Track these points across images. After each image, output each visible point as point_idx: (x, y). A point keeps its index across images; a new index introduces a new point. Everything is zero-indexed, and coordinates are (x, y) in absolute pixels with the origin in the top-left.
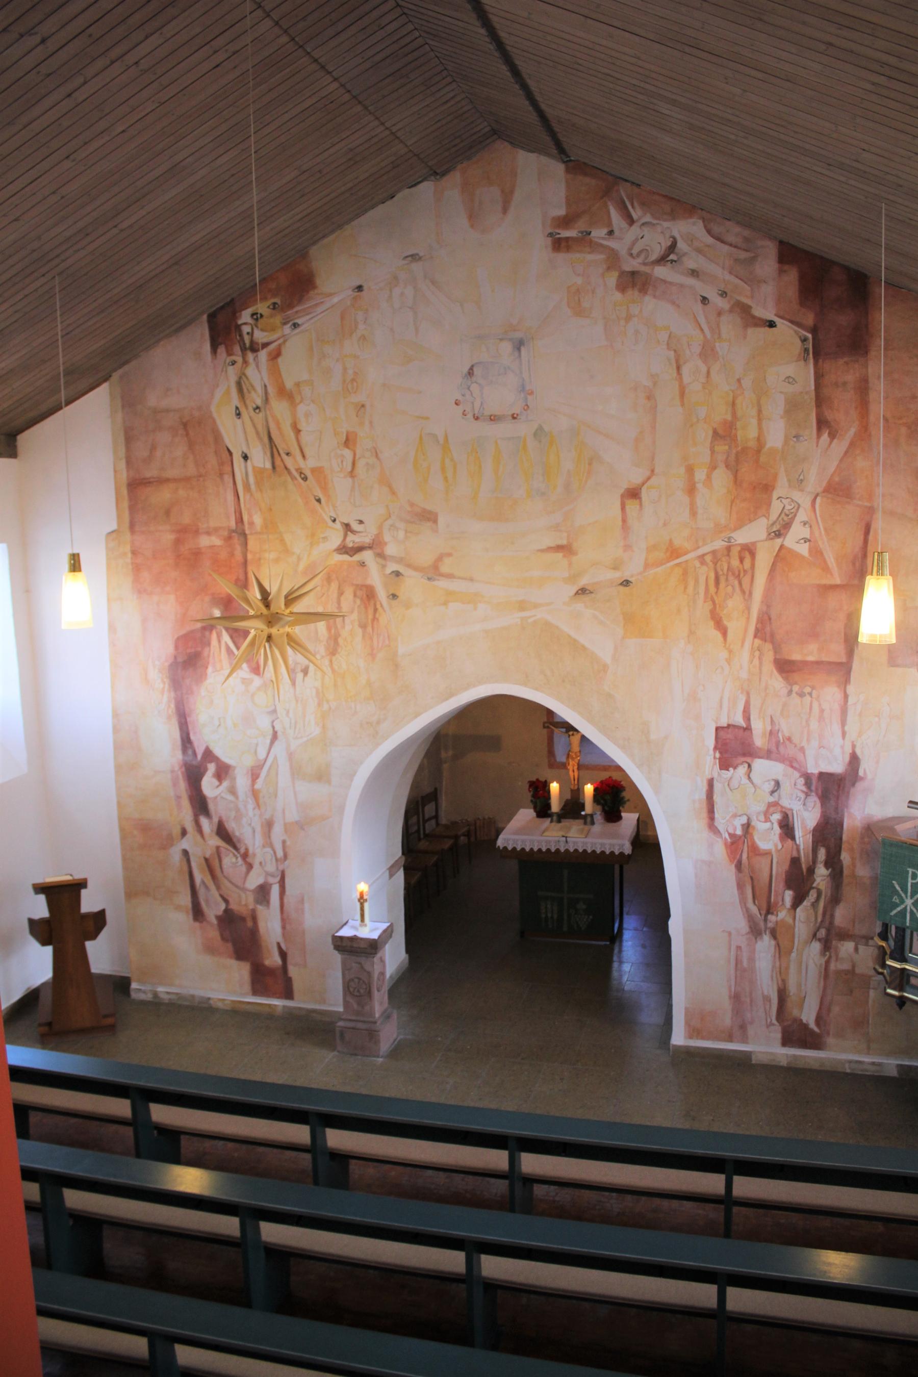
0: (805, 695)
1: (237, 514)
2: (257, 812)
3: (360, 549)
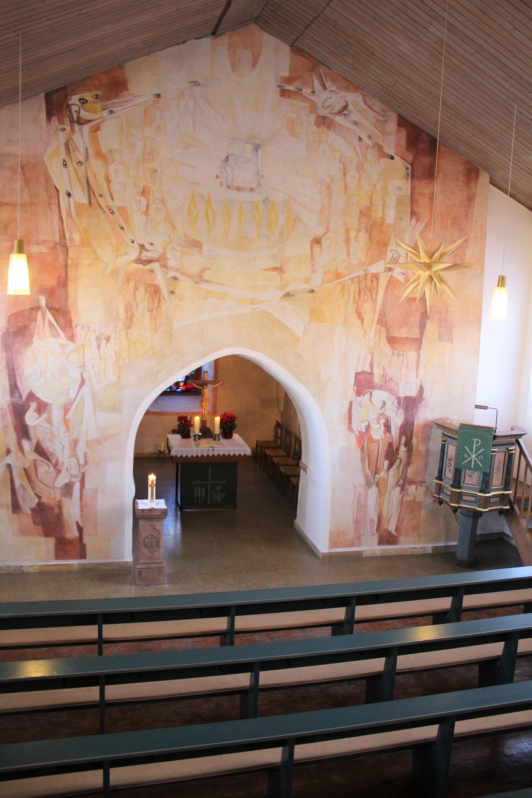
0: (400, 356)
1: (61, 233)
3: (150, 261)
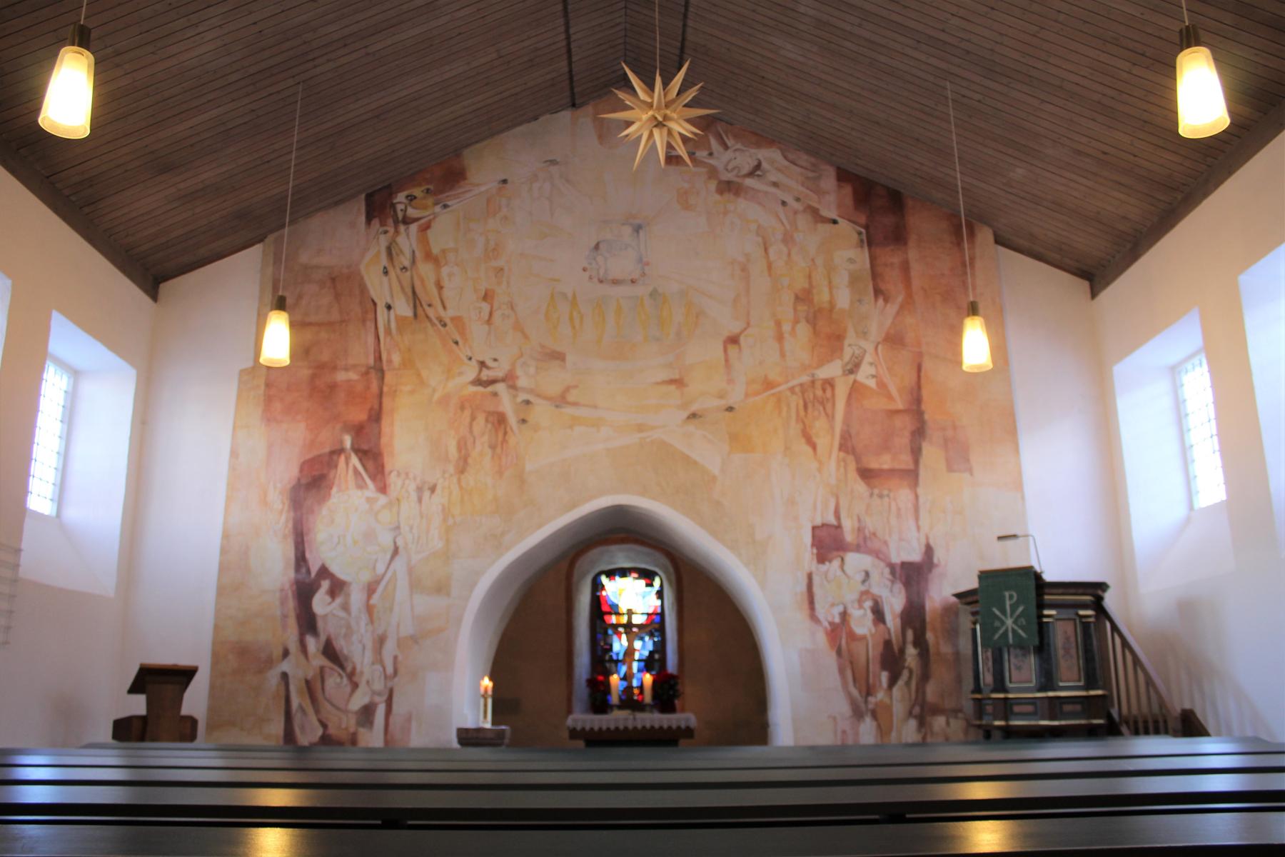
3: (493, 382)
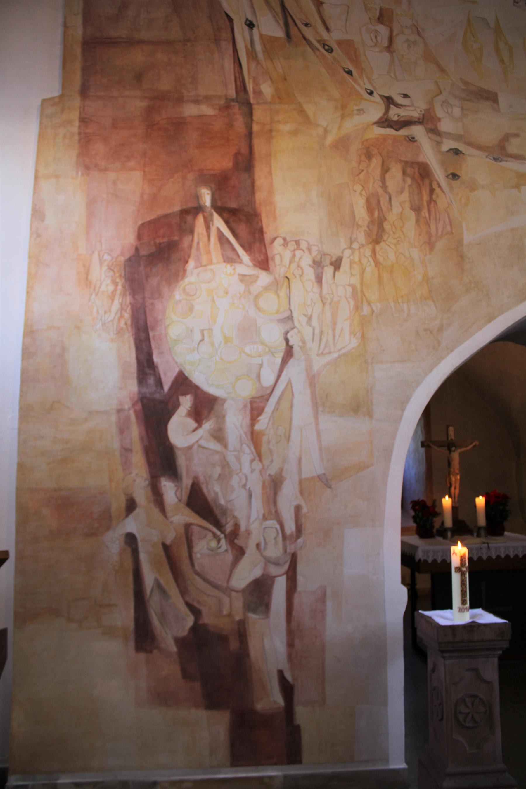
1: (238, 83)
2: (257, 465)
3: (407, 123)
